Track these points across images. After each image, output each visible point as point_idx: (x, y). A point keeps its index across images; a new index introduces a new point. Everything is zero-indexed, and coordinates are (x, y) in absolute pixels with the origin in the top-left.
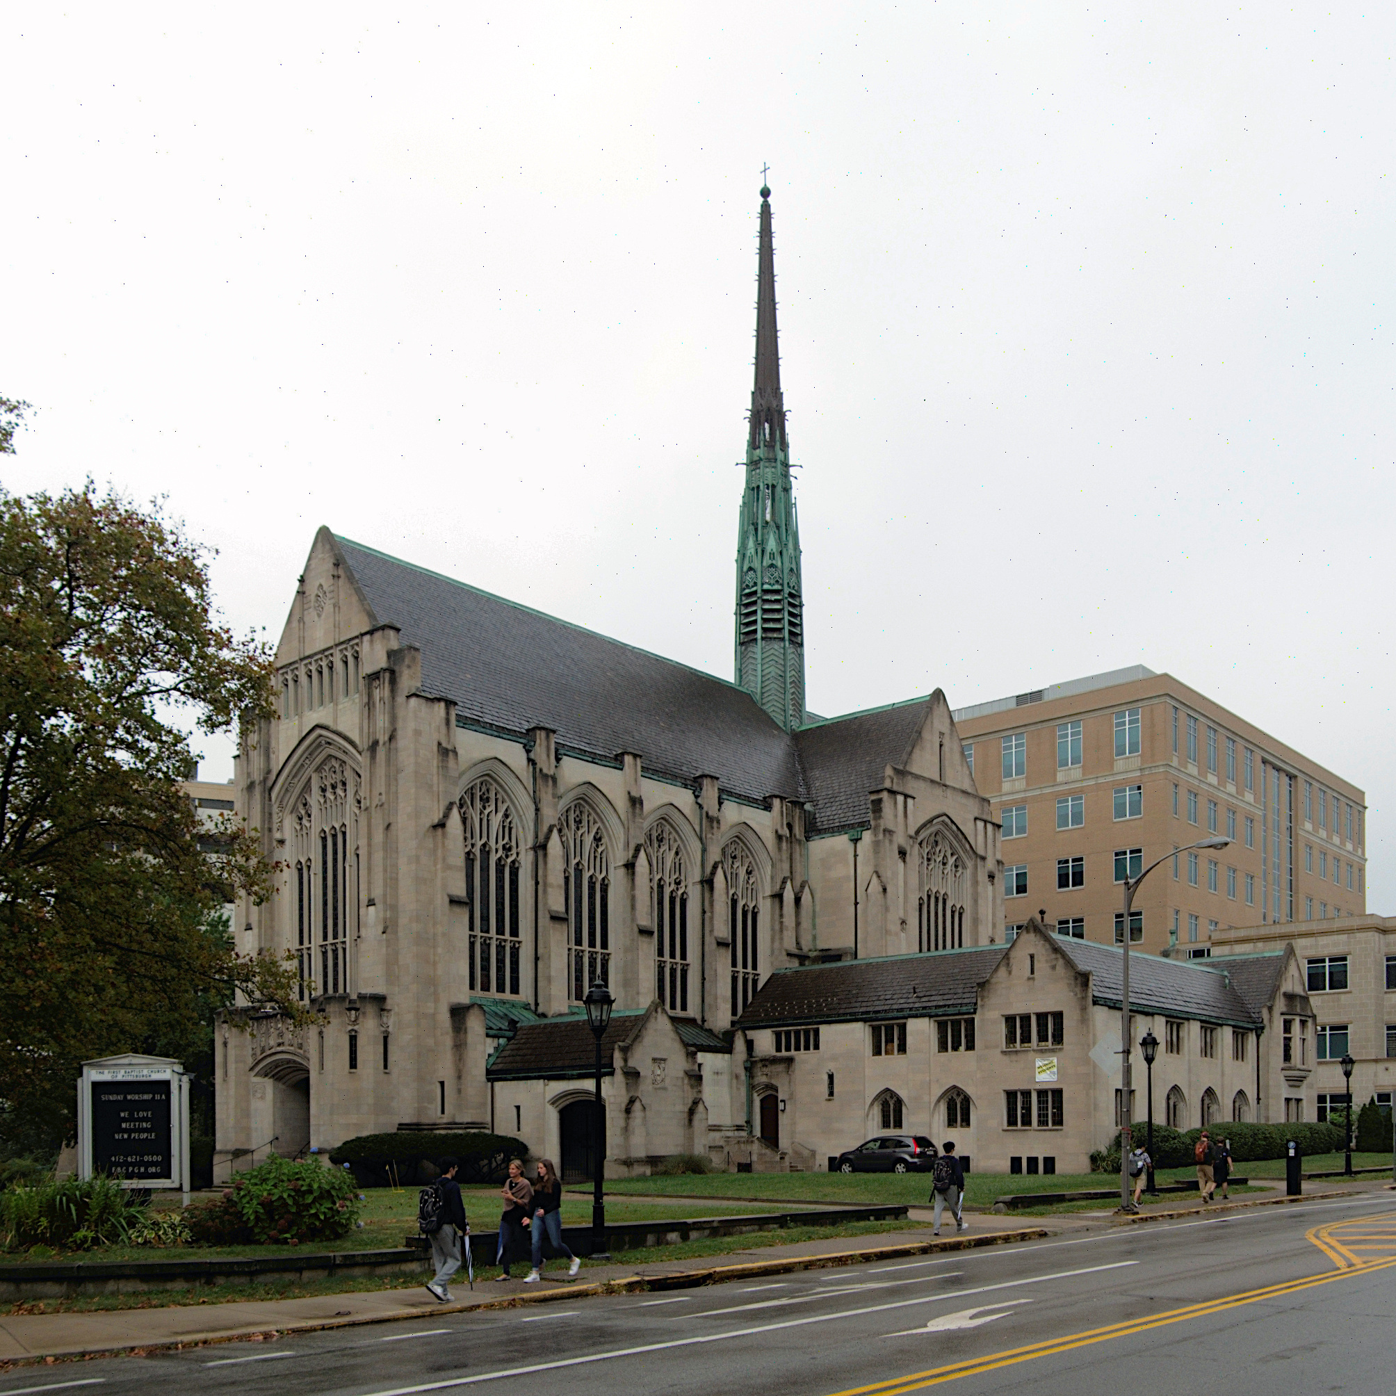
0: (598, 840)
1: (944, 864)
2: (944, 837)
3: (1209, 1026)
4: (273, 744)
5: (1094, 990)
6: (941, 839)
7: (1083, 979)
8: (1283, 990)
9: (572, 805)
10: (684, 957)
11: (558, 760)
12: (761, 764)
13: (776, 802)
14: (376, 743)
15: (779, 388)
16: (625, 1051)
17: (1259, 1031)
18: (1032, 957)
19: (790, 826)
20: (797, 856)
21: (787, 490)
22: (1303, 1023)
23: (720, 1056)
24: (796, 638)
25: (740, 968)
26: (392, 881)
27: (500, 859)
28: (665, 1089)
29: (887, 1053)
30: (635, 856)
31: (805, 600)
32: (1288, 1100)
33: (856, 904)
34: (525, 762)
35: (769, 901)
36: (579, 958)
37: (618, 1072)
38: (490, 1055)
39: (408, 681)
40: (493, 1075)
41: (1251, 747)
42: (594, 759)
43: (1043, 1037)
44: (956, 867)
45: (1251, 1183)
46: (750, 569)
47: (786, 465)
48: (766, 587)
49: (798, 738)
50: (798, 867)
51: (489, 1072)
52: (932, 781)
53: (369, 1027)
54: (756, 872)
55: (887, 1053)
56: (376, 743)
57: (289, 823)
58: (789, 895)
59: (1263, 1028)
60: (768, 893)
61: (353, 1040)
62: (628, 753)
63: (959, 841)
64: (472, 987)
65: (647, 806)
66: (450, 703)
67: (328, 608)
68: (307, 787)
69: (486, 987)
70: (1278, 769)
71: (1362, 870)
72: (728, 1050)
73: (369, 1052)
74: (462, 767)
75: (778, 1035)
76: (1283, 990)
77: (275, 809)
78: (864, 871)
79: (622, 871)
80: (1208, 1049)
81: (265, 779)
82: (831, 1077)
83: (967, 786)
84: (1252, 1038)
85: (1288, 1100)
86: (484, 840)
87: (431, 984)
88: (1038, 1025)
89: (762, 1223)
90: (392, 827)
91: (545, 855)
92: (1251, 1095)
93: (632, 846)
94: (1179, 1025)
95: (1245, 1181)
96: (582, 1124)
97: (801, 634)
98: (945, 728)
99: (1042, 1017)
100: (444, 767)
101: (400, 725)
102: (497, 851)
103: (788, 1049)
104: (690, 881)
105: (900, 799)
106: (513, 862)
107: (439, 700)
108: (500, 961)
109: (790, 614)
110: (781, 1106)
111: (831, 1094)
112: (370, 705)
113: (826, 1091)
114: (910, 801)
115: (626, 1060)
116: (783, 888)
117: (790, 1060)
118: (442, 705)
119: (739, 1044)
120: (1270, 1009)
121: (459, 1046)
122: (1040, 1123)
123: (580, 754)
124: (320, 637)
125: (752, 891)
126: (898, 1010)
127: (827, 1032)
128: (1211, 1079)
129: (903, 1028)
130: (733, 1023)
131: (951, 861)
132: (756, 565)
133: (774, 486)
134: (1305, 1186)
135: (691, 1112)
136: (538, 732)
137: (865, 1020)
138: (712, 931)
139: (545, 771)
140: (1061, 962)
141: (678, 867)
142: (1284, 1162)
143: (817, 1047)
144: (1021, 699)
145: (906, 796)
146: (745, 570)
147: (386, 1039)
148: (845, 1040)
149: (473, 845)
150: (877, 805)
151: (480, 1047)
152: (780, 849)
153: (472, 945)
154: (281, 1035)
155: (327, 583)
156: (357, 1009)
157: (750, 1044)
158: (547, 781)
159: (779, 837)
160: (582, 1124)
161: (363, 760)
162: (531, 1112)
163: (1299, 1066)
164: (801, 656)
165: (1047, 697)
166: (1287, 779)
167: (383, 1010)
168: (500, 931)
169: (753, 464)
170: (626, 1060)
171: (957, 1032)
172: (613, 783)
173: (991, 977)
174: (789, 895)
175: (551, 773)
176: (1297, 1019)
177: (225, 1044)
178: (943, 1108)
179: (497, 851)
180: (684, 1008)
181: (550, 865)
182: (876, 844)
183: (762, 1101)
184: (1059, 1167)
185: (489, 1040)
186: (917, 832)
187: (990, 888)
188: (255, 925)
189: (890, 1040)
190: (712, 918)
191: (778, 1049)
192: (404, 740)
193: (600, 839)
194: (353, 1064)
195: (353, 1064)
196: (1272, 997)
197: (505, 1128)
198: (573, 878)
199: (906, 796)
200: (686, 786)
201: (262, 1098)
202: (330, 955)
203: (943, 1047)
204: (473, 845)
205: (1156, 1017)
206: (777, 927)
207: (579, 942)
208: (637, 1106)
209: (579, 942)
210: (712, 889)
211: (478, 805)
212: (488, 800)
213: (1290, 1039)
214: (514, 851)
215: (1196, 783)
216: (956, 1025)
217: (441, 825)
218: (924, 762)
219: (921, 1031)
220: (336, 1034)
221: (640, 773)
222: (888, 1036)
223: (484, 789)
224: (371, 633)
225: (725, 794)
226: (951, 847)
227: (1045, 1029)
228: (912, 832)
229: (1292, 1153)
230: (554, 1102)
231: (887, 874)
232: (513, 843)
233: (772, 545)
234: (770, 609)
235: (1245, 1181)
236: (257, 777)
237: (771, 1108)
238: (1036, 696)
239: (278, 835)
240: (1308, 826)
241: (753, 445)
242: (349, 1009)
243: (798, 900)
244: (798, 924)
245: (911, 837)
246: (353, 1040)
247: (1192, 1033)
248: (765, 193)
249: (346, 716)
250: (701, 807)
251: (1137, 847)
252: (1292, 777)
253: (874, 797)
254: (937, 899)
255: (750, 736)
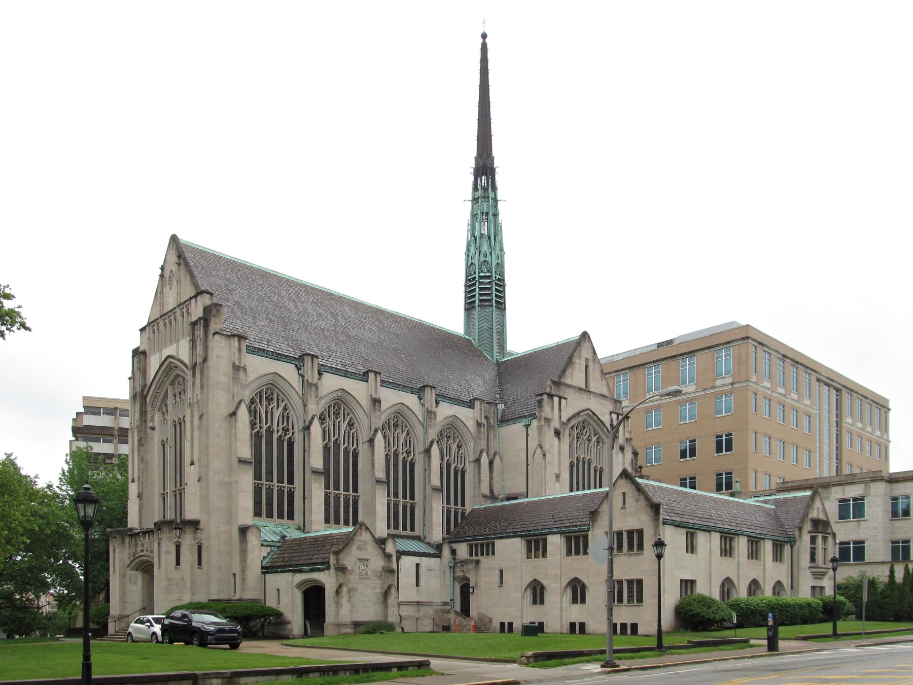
0: (459, 447)
1: (589, 441)
2: (589, 424)
3: (754, 542)
4: (148, 370)
5: (663, 515)
6: (584, 426)
7: (655, 508)
8: (810, 516)
9: (332, 403)
10: (412, 498)
11: (320, 374)
12: (479, 383)
13: (477, 404)
14: (196, 364)
15: (491, 154)
16: (337, 553)
17: (792, 542)
18: (624, 494)
19: (486, 417)
20: (491, 436)
21: (496, 215)
22: (825, 539)
23: (432, 559)
24: (501, 306)
25: (332, 490)
26: (205, 450)
27: (280, 436)
28: (368, 579)
29: (535, 557)
30: (375, 435)
31: (507, 282)
32: (813, 588)
33: (527, 465)
34: (297, 376)
35: (422, 455)
36: (449, 512)
37: (332, 567)
38: (264, 558)
39: (214, 326)
40: (267, 570)
41: (809, 371)
42: (346, 374)
43: (631, 547)
44: (598, 442)
45: (752, 642)
46: (472, 264)
47: (495, 200)
48: (481, 274)
49: (499, 364)
50: (492, 443)
51: (263, 568)
52: (580, 389)
53: (188, 541)
54: (356, 425)
55: (535, 557)
56: (196, 364)
57: (157, 417)
58: (485, 460)
59: (795, 541)
60: (472, 459)
61: (178, 547)
62: (371, 371)
63: (599, 426)
64: (388, 528)
65: (384, 405)
66: (241, 338)
67: (175, 283)
68: (166, 396)
69: (396, 528)
70: (829, 385)
71: (887, 448)
72: (438, 556)
73: (188, 555)
74: (250, 379)
75: (471, 546)
76: (810, 516)
77: (149, 409)
78: (533, 444)
79: (366, 445)
80: (754, 554)
81: (143, 391)
82: (501, 572)
83: (605, 392)
84: (787, 549)
85: (813, 588)
86: (337, 436)
87: (230, 514)
88: (628, 538)
89: (401, 666)
90: (204, 416)
91: (309, 434)
92: (786, 583)
93: (373, 429)
94: (731, 540)
95: (746, 641)
96: (314, 599)
97: (505, 303)
98: (590, 356)
99: (630, 533)
100: (235, 379)
101: (210, 352)
102: (278, 431)
103: (477, 555)
104: (417, 451)
105: (556, 399)
106: (290, 438)
107: (233, 336)
108: (404, 514)
109: (496, 290)
110: (471, 590)
111: (502, 583)
112: (193, 342)
113: (498, 581)
114: (563, 401)
115: (338, 560)
116: (480, 456)
117: (478, 562)
118: (236, 339)
119: (446, 552)
120: (800, 529)
121: (244, 552)
122: (629, 601)
123: (335, 371)
124: (171, 302)
125: (463, 459)
126: (542, 529)
127: (499, 544)
128: (765, 574)
129: (545, 541)
130: (444, 539)
131: (594, 439)
132: (476, 261)
133: (487, 214)
134: (781, 644)
135: (386, 594)
136: (306, 358)
137: (522, 536)
138: (430, 482)
139: (310, 381)
140: (642, 496)
141: (408, 442)
142: (765, 629)
143: (493, 554)
144: (660, 345)
145: (560, 398)
146: (469, 266)
147: (200, 548)
148: (510, 549)
149: (261, 428)
150: (540, 402)
151: (257, 552)
152: (479, 432)
153: (389, 505)
154: (142, 545)
155: (174, 268)
156: (180, 529)
157: (453, 552)
158: (311, 388)
159: (479, 425)
160: (314, 599)
161: (189, 373)
162: (285, 594)
163: (821, 565)
164: (504, 316)
165: (676, 342)
166: (835, 391)
167: (197, 529)
168: (456, 504)
169: (475, 200)
170: (338, 560)
171: (577, 543)
172: (358, 390)
173: (599, 507)
174: (485, 460)
175: (315, 382)
176: (820, 536)
177: (114, 551)
178: (569, 591)
179: (278, 431)
180: (412, 529)
181: (312, 440)
182: (540, 428)
183: (461, 587)
184: (640, 630)
185: (264, 548)
186: (569, 420)
187: (620, 455)
188: (136, 479)
189: (537, 549)
190: (430, 474)
191: (471, 555)
192: (212, 361)
193: (353, 425)
194: (178, 563)
195: (178, 563)
196: (803, 520)
197: (271, 603)
198: (446, 467)
199: (560, 398)
200: (413, 393)
201: (135, 584)
202: (178, 496)
203: (569, 553)
204: (261, 428)
205: (713, 533)
206: (477, 480)
207: (448, 502)
208: (345, 589)
209: (448, 502)
210: (429, 457)
211: (264, 402)
212: (272, 399)
213: (815, 548)
214: (412, 453)
215: (769, 392)
216: (577, 539)
217: (234, 414)
218: (575, 377)
219: (555, 543)
220: (168, 546)
221: (379, 383)
222: (536, 546)
223: (269, 392)
224: (195, 297)
225: (441, 397)
226: (594, 430)
227: (632, 541)
228: (564, 419)
229: (770, 623)
230: (299, 586)
231: (547, 446)
232: (290, 427)
233: (485, 248)
234: (485, 290)
235: (746, 641)
236: (138, 389)
237: (466, 592)
238: (669, 342)
239: (150, 425)
240: (849, 420)
241: (475, 188)
242: (176, 529)
243: (491, 463)
244: (491, 478)
245: (564, 423)
246: (178, 547)
247: (742, 544)
248: (484, 36)
249: (182, 350)
250: (303, 376)
251: (729, 432)
252: (838, 390)
253: (539, 398)
254: (584, 462)
255: (482, 368)
